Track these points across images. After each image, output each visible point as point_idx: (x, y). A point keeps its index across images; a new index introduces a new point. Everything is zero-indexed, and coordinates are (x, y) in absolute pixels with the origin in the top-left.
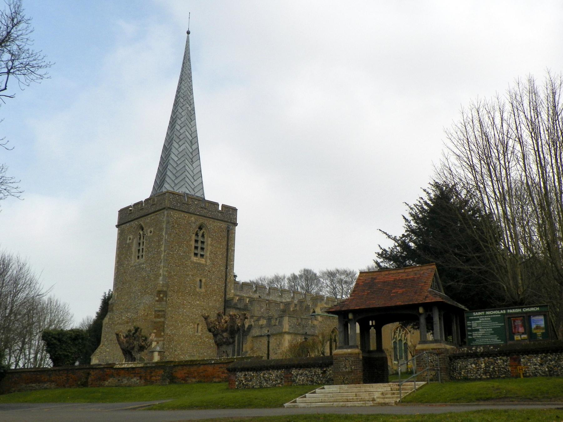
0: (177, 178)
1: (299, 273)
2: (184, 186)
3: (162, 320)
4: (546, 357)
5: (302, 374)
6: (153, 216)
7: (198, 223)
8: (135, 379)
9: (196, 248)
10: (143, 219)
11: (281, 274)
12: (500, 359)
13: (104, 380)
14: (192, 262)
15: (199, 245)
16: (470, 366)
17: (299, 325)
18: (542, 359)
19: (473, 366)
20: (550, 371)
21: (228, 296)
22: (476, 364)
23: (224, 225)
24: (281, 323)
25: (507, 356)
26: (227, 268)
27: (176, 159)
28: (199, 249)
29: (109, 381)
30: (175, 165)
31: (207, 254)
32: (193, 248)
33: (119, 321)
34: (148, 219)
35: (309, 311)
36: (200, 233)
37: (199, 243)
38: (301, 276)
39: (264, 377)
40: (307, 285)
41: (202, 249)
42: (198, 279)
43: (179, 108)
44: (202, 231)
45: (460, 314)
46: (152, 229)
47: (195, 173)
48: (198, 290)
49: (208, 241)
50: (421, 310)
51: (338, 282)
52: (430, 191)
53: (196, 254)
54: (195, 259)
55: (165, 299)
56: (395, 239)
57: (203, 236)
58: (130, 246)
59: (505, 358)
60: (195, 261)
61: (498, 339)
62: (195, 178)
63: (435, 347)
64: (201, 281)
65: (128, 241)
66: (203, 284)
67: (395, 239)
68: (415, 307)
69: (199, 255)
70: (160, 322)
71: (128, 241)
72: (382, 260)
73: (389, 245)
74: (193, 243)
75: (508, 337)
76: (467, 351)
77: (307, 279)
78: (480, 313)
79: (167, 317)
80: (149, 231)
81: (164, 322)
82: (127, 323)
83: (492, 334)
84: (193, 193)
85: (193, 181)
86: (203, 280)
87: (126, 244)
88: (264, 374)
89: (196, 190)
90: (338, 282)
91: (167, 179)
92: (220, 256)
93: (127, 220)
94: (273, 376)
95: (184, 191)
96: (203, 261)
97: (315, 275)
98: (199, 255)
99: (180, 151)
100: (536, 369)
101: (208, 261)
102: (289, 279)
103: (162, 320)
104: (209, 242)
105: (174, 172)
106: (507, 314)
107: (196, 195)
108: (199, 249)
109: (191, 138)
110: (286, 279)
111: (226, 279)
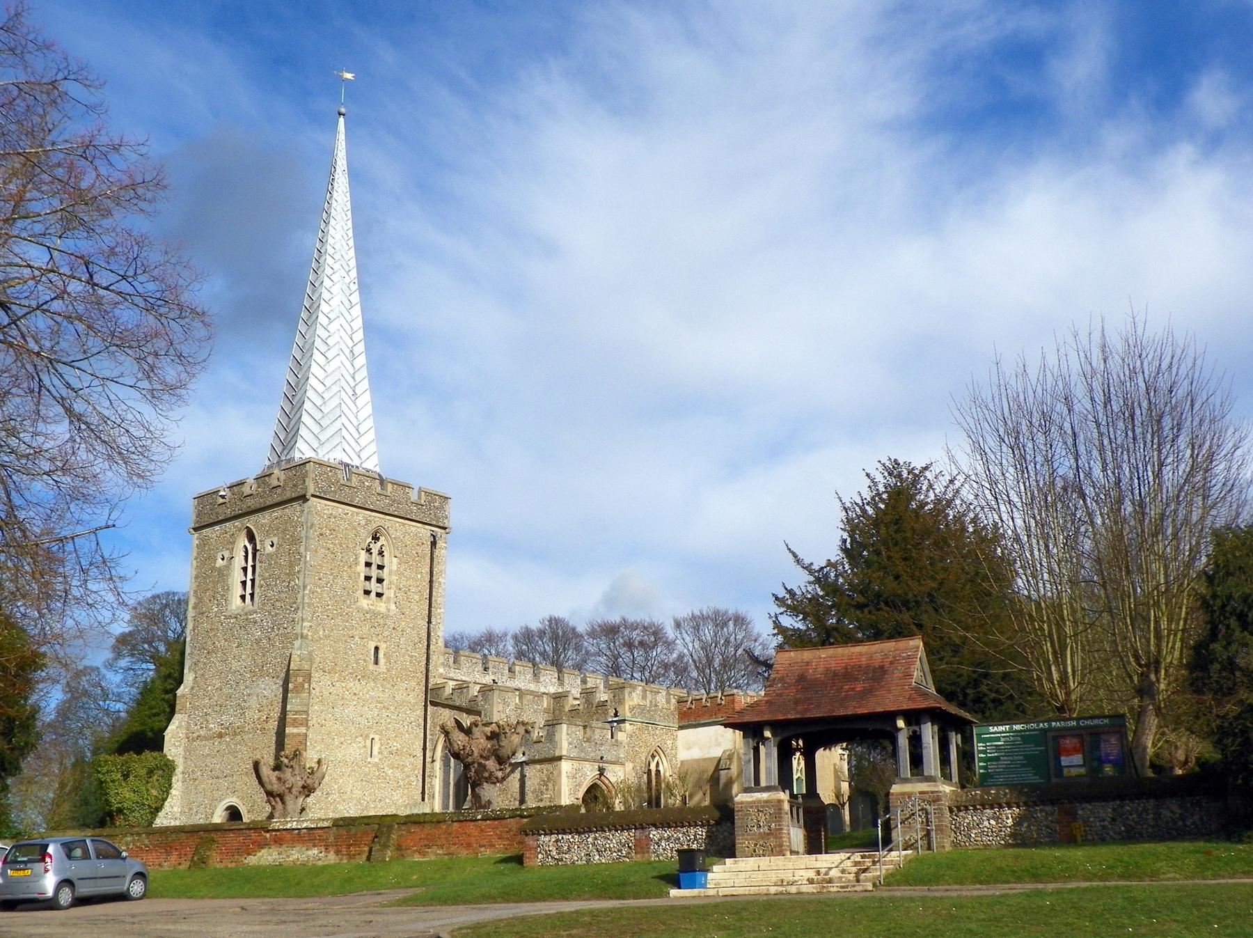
0: (323, 429)
1: (540, 626)
2: (339, 447)
3: (303, 730)
4: (1122, 807)
5: (668, 839)
6: (277, 512)
7: (372, 527)
8: (315, 851)
9: (368, 578)
10: (252, 518)
11: (498, 628)
12: (1041, 811)
13: (249, 854)
14: (359, 610)
15: (374, 572)
16: (986, 823)
17: (588, 740)
18: (1114, 810)
19: (993, 822)
20: (1127, 832)
21: (432, 681)
22: (997, 819)
23: (425, 532)
24: (551, 737)
25: (1053, 804)
26: (429, 622)
27: (320, 388)
28: (374, 580)
29: (259, 854)
30: (319, 402)
31: (389, 593)
32: (362, 578)
33: (202, 733)
34: (265, 518)
35: (606, 713)
36: (375, 548)
37: (374, 567)
38: (542, 633)
39: (593, 844)
40: (556, 650)
41: (380, 581)
42: (372, 646)
43: (326, 279)
44: (379, 544)
45: (963, 726)
46: (275, 540)
47: (361, 419)
48: (372, 667)
49: (391, 563)
50: (901, 723)
51: (625, 644)
52: (879, 478)
53: (367, 592)
54: (364, 602)
55: (306, 686)
56: (808, 568)
57: (381, 553)
58: (223, 574)
59: (1049, 809)
60: (366, 607)
61: (1035, 774)
62: (362, 430)
63: (926, 789)
64: (377, 648)
65: (220, 563)
66: (381, 655)
67: (808, 568)
68: (891, 716)
69: (373, 594)
70: (299, 735)
71: (220, 563)
72: (782, 610)
73: (800, 582)
74: (361, 568)
75: (1052, 772)
76: (982, 796)
77: (555, 638)
78: (1001, 728)
79: (310, 724)
80: (268, 542)
81: (306, 735)
82: (220, 736)
83: (1023, 766)
84: (356, 462)
85: (356, 436)
86: (383, 647)
87: (213, 569)
88: (596, 839)
89: (364, 455)
90: (625, 644)
91: (303, 431)
92: (416, 597)
93: (214, 519)
94: (613, 844)
95: (339, 458)
96: (381, 606)
97: (574, 629)
98: (373, 594)
99: (329, 371)
100: (1104, 827)
101: (393, 607)
102: (515, 637)
103: (303, 730)
104: (395, 567)
105: (318, 416)
106: (1050, 729)
107: (364, 466)
108: (374, 580)
109: (350, 344)
110: (509, 637)
111: (428, 646)
